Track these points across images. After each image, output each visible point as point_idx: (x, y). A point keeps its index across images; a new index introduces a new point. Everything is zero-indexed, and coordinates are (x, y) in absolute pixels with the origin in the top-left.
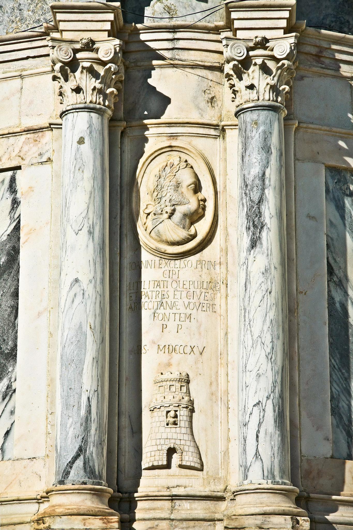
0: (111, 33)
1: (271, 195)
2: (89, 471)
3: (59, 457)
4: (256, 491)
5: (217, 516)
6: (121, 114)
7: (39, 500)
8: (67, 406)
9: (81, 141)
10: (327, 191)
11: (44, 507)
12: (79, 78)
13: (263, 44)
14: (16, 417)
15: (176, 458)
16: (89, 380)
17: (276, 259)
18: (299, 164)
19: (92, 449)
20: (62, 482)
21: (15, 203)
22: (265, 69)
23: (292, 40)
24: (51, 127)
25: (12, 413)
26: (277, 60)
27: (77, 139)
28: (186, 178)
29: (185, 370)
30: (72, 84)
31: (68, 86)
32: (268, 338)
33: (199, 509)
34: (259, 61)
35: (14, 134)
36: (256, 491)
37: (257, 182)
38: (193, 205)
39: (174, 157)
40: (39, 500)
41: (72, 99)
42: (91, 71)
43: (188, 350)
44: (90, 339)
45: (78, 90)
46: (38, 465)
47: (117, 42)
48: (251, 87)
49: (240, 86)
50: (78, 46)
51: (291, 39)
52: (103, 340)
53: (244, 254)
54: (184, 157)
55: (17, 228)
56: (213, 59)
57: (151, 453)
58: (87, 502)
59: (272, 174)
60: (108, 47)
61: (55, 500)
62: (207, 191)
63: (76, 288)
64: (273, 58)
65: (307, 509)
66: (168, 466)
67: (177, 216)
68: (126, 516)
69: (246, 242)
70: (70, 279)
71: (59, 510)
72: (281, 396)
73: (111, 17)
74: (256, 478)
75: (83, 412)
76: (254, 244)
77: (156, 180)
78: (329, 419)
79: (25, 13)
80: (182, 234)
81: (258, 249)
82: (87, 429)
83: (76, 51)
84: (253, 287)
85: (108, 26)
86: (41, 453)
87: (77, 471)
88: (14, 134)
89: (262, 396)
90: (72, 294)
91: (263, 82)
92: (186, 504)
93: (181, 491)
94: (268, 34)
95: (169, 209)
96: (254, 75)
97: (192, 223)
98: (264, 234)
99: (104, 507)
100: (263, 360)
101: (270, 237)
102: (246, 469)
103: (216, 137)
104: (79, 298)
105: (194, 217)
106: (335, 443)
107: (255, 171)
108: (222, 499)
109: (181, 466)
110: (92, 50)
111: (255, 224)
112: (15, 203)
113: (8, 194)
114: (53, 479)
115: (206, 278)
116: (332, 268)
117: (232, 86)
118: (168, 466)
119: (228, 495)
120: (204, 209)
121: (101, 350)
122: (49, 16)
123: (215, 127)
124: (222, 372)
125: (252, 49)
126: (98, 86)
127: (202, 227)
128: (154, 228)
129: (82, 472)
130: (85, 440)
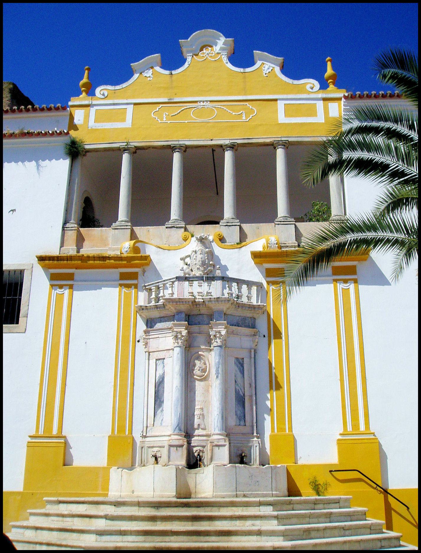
0: (186, 329)
33: (204, 438)
65: (229, 438)
69: (215, 377)
78: (235, 417)
88: (164, 350)
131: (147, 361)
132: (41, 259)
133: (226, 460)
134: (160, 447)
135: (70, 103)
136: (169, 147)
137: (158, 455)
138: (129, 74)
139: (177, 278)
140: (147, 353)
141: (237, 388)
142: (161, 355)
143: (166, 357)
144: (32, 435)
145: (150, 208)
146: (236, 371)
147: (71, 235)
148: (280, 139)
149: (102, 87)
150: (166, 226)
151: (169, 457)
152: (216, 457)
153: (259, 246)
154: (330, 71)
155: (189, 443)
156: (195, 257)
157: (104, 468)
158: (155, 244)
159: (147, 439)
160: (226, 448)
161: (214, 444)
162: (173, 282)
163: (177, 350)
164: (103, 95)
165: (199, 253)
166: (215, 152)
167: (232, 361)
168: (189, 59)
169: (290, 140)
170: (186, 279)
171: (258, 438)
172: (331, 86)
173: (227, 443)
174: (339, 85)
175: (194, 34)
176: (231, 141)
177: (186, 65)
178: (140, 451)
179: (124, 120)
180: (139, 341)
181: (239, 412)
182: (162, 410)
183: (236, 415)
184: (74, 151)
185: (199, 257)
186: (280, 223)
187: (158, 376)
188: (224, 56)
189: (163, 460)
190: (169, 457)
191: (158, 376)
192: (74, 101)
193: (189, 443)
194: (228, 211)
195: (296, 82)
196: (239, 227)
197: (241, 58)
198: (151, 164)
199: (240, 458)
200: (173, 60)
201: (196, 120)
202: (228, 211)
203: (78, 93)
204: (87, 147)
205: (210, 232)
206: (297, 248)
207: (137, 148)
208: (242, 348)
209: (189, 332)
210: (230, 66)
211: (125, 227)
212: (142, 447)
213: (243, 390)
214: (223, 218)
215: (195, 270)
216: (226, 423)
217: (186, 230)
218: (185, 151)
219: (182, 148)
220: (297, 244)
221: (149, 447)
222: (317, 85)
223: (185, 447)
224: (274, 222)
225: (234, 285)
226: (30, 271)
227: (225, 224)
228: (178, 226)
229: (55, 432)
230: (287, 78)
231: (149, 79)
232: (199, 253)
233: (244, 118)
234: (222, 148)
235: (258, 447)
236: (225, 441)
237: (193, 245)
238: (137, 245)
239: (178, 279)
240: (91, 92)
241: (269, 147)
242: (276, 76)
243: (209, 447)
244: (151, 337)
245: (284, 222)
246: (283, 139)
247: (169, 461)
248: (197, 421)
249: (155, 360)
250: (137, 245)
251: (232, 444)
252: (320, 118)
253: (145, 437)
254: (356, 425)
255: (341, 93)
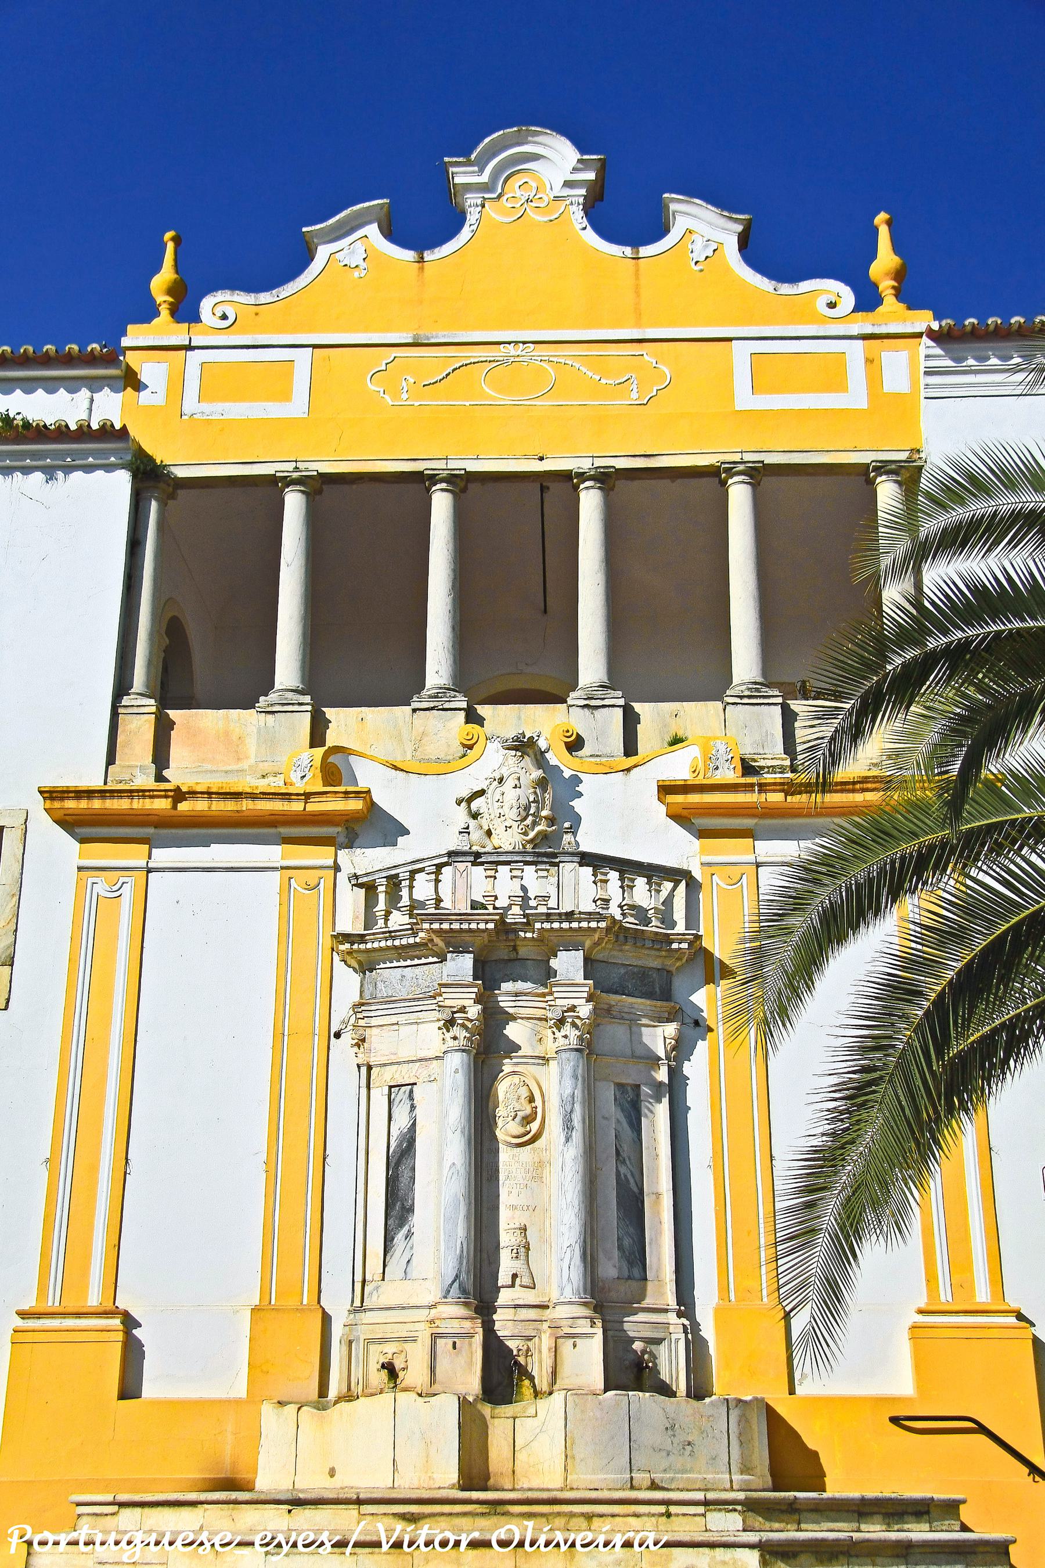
0: (477, 1001)
1: (578, 1107)
2: (463, 1291)
3: (443, 1281)
4: (570, 1303)
5: (544, 1318)
6: (482, 1049)
7: (430, 1307)
8: (447, 1248)
9: (456, 1071)
10: (615, 1099)
11: (433, 1311)
12: (456, 1031)
13: (573, 1008)
14: (414, 1251)
15: (518, 1281)
16: (461, 1231)
17: (581, 1150)
18: (598, 1083)
19: (463, 1276)
20: (445, 1297)
21: (413, 1107)
22: (574, 1025)
23: (591, 1007)
24: (437, 1058)
25: (412, 1248)
26: (582, 1019)
27: (453, 1070)
28: (524, 1092)
29: (524, 1222)
30: (451, 1034)
31: (448, 1035)
32: (576, 1203)
33: (532, 1314)
34: (570, 1020)
35: (413, 1061)
36: (570, 1303)
37: (570, 1099)
38: (528, 1111)
39: (516, 1079)
40: (430, 1307)
41: (451, 1043)
42: (463, 1026)
43: (525, 1208)
44: (462, 1203)
45: (455, 1038)
46: (427, 1283)
47: (480, 1007)
48: (566, 1037)
49: (558, 1035)
50: (455, 1010)
51: (590, 1006)
52: (470, 1164)
53: (561, 1147)
54: (523, 1078)
55: (414, 1124)
56: (539, 1013)
57: (504, 1278)
58: (462, 1311)
59: (578, 1093)
60: (474, 1011)
61: (441, 1308)
62: (538, 1102)
63: (453, 1170)
64: (578, 1017)
65: (602, 1314)
66: (513, 1286)
67: (518, 1119)
68: (486, 1318)
69: (563, 1139)
70: (450, 1163)
71: (444, 1316)
72: (585, 1241)
73: (476, 990)
74: (569, 1295)
75: (458, 1252)
76: (567, 1140)
77: (507, 1090)
78: (616, 1253)
79: (420, 981)
80: (522, 1130)
81: (569, 1144)
82: (461, 1263)
83: (454, 1013)
84: (567, 1169)
85: (473, 996)
86: (430, 1275)
87: (455, 1290)
88: (413, 1061)
89: (572, 1241)
90: (450, 1174)
91: (573, 1034)
92: (524, 1311)
93: (521, 1302)
94: (575, 1002)
95: (513, 1114)
96: (567, 1029)
97: (528, 1123)
98: (574, 1134)
99: (472, 1314)
100: (573, 1217)
101: (577, 1136)
102: (562, 1289)
103: (543, 1065)
104: (455, 1175)
105: (528, 1120)
106: (620, 1269)
107: (568, 1091)
108: (548, 1307)
109: (521, 1286)
110: (464, 1012)
111: (568, 1126)
112: (413, 1107)
113: (408, 1101)
114: (440, 1295)
115: (537, 1160)
116: (629, 1118)
117: (554, 1033)
118: (513, 1286)
119: (551, 1305)
120: (536, 1113)
121: (469, 1210)
122: (437, 986)
123: (543, 1058)
124: (547, 1224)
125: (566, 1011)
126: (468, 1035)
127: (535, 1126)
128: (506, 1129)
129: (458, 1291)
130: (459, 1270)
131: (364, 1091)
132: (50, 794)
133: (596, 1377)
134: (405, 1340)
135: (125, 342)
136: (418, 477)
137: (398, 1364)
138: (301, 257)
139: (450, 854)
140: (364, 1070)
141: (623, 1170)
142: (403, 1074)
143: (419, 1082)
144: (26, 1307)
145: (364, 653)
146: (618, 1121)
147: (139, 729)
148: (737, 458)
149: (220, 296)
150: (415, 705)
151: (433, 1370)
152: (564, 1371)
153: (679, 766)
154: (885, 261)
155: (489, 1328)
156: (498, 796)
157: (236, 1403)
158: (383, 758)
159: (368, 1317)
160: (596, 1345)
161: (561, 1333)
162: (439, 867)
163: (457, 1060)
164: (224, 317)
165: (510, 783)
166: (550, 493)
167: (607, 1094)
168: (472, 217)
169: (770, 459)
170: (476, 859)
171: (680, 1314)
172: (890, 302)
173: (599, 1331)
174: (910, 296)
175: (487, 140)
176: (599, 463)
177: (465, 233)
178: (345, 1353)
179: (285, 396)
180: (338, 1035)
181: (627, 1242)
182: (409, 1235)
183: (620, 1247)
184: (148, 476)
185: (511, 795)
186: (738, 700)
187: (395, 1133)
188: (574, 208)
189: (415, 1374)
190: (433, 1370)
191: (395, 1133)
192: (135, 335)
193: (489, 1328)
194: (591, 665)
195: (786, 288)
196: (620, 711)
197: (624, 213)
198: (367, 519)
199: (629, 1371)
200: (426, 221)
201: (494, 399)
202: (591, 665)
203: (147, 313)
204: (181, 473)
205: (543, 722)
206: (790, 775)
207: (327, 479)
208: (633, 1056)
209: (484, 1010)
210: (591, 238)
211: (296, 708)
212: (350, 1342)
213: (637, 1177)
214: (574, 686)
215: (498, 829)
216: (592, 1272)
217: (473, 717)
218: (464, 490)
219: (458, 481)
220: (788, 763)
221: (370, 1341)
222: (847, 297)
223: (478, 1339)
224: (721, 700)
225: (613, 876)
226: (19, 833)
227: (583, 702)
228: (447, 706)
229: (94, 1299)
230: (759, 276)
231: (356, 274)
232: (510, 783)
233: (634, 395)
234: (570, 480)
235: (682, 1345)
236: (593, 1324)
237: (494, 759)
238: (331, 759)
239: (453, 855)
240: (185, 310)
241: (704, 480)
242: (728, 270)
243: (546, 1341)
244: (374, 1022)
245: (754, 695)
246: (747, 457)
247: (433, 1381)
248: (507, 1265)
249: (386, 1090)
250: (331, 759)
251: (610, 1333)
252: (855, 396)
253: (361, 1309)
254: (963, 1285)
255: (924, 320)
